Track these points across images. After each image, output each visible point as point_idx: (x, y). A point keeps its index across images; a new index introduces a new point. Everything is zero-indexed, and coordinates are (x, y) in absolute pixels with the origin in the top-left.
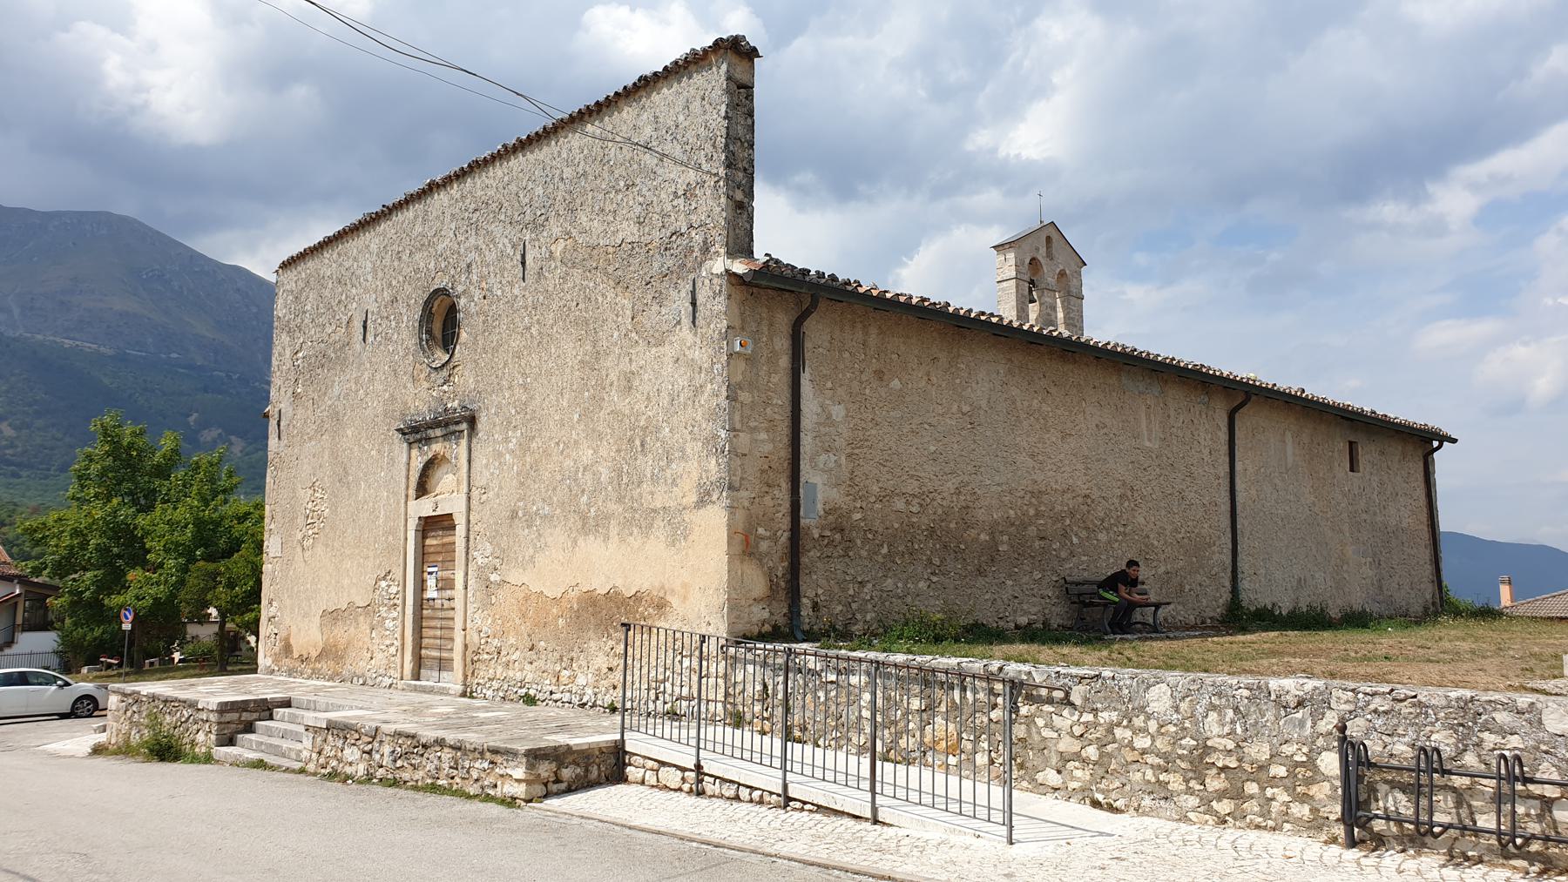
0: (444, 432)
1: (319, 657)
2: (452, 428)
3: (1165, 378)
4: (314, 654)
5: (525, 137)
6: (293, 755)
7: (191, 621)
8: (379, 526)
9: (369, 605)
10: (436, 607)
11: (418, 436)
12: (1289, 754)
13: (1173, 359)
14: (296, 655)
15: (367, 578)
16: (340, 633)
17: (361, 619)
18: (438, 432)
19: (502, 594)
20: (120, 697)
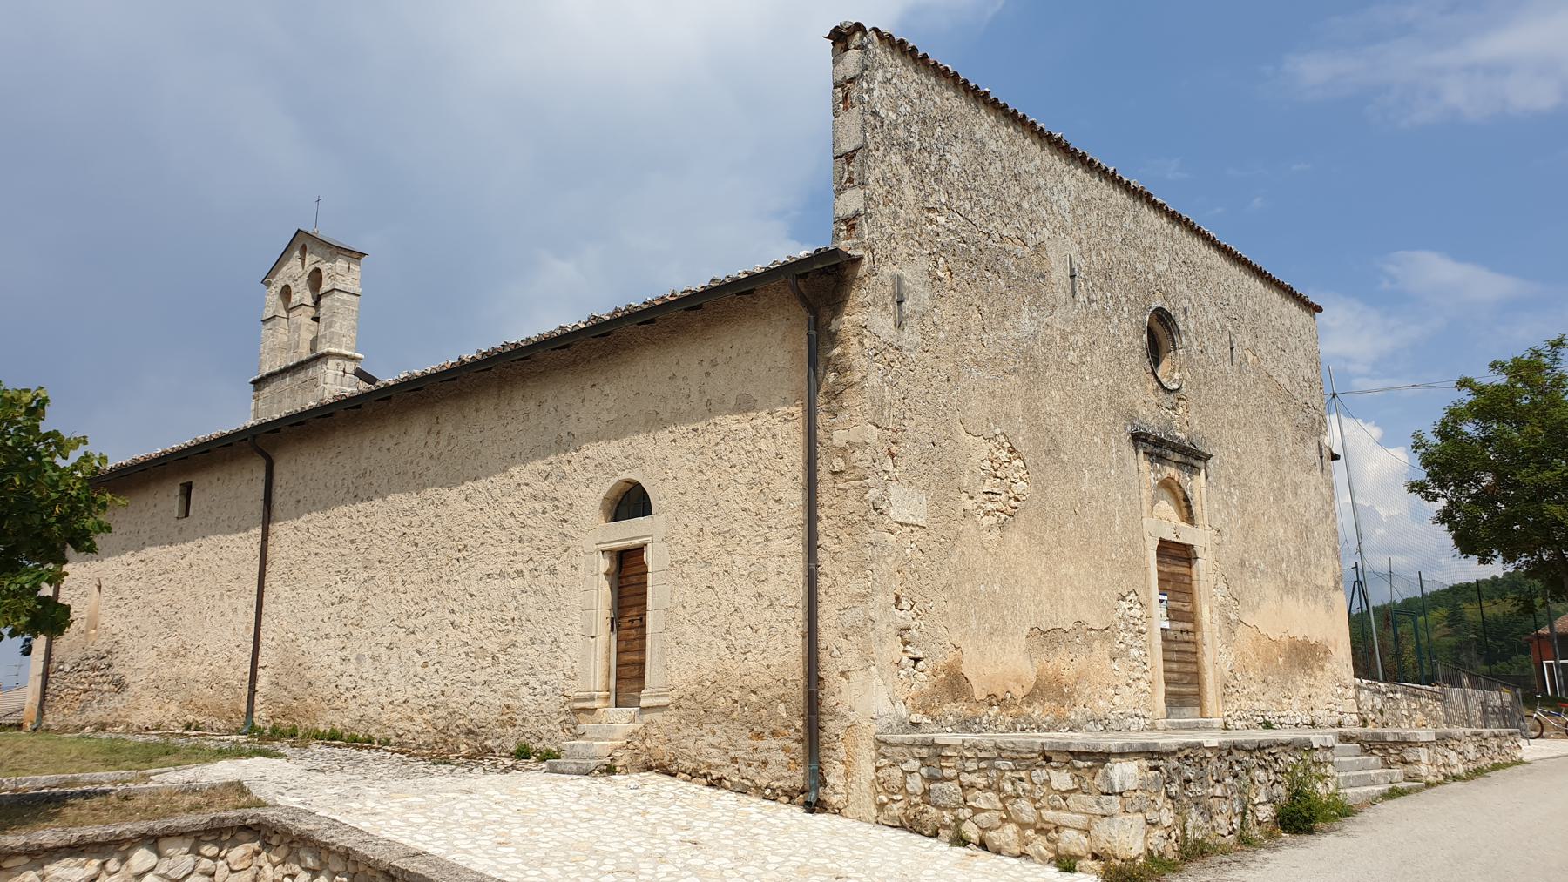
0: (1184, 460)
1: (1030, 698)
2: (1192, 460)
3: (787, 315)
4: (1019, 693)
5: (973, 84)
6: (1382, 780)
7: (46, 582)
8: (1115, 533)
9: (1107, 629)
10: (1170, 638)
11: (1158, 450)
12: (990, 794)
13: (1466, 557)
14: (979, 694)
15: (1103, 593)
16: (1064, 664)
17: (1096, 644)
18: (1178, 457)
19: (1240, 630)
20: (1145, 764)
